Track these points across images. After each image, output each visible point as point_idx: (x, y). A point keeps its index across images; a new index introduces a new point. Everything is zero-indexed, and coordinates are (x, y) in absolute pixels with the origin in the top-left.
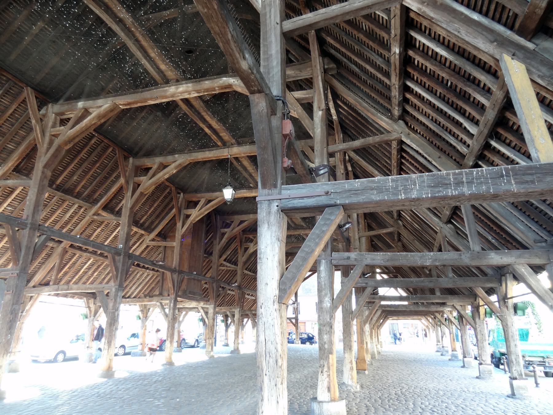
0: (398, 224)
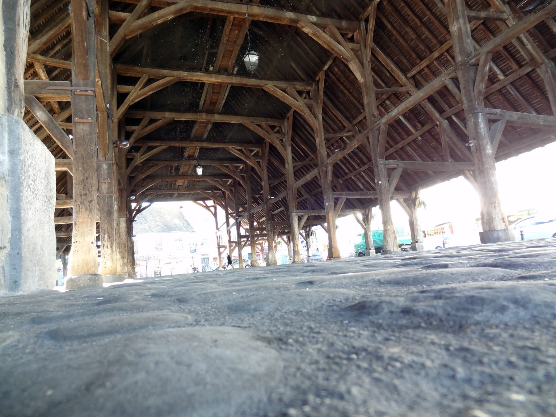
0: (355, 129)
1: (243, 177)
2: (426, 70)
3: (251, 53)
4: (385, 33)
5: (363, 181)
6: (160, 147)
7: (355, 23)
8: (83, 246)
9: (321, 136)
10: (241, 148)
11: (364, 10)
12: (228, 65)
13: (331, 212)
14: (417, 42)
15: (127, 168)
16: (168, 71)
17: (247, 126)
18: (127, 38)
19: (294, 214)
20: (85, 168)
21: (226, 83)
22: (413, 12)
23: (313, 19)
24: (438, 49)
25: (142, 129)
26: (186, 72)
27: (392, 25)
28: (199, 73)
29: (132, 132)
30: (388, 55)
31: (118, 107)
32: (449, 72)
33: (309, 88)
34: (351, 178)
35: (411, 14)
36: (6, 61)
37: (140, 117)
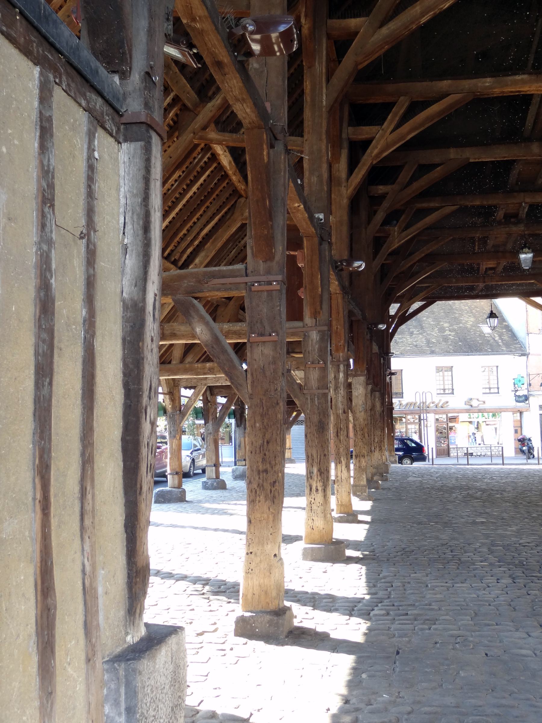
8: (261, 562)
15: (374, 260)
16: (449, 81)
18: (360, 67)
20: (265, 424)
25: (402, 190)
26: (489, 80)
28: (518, 77)
36: (127, 546)
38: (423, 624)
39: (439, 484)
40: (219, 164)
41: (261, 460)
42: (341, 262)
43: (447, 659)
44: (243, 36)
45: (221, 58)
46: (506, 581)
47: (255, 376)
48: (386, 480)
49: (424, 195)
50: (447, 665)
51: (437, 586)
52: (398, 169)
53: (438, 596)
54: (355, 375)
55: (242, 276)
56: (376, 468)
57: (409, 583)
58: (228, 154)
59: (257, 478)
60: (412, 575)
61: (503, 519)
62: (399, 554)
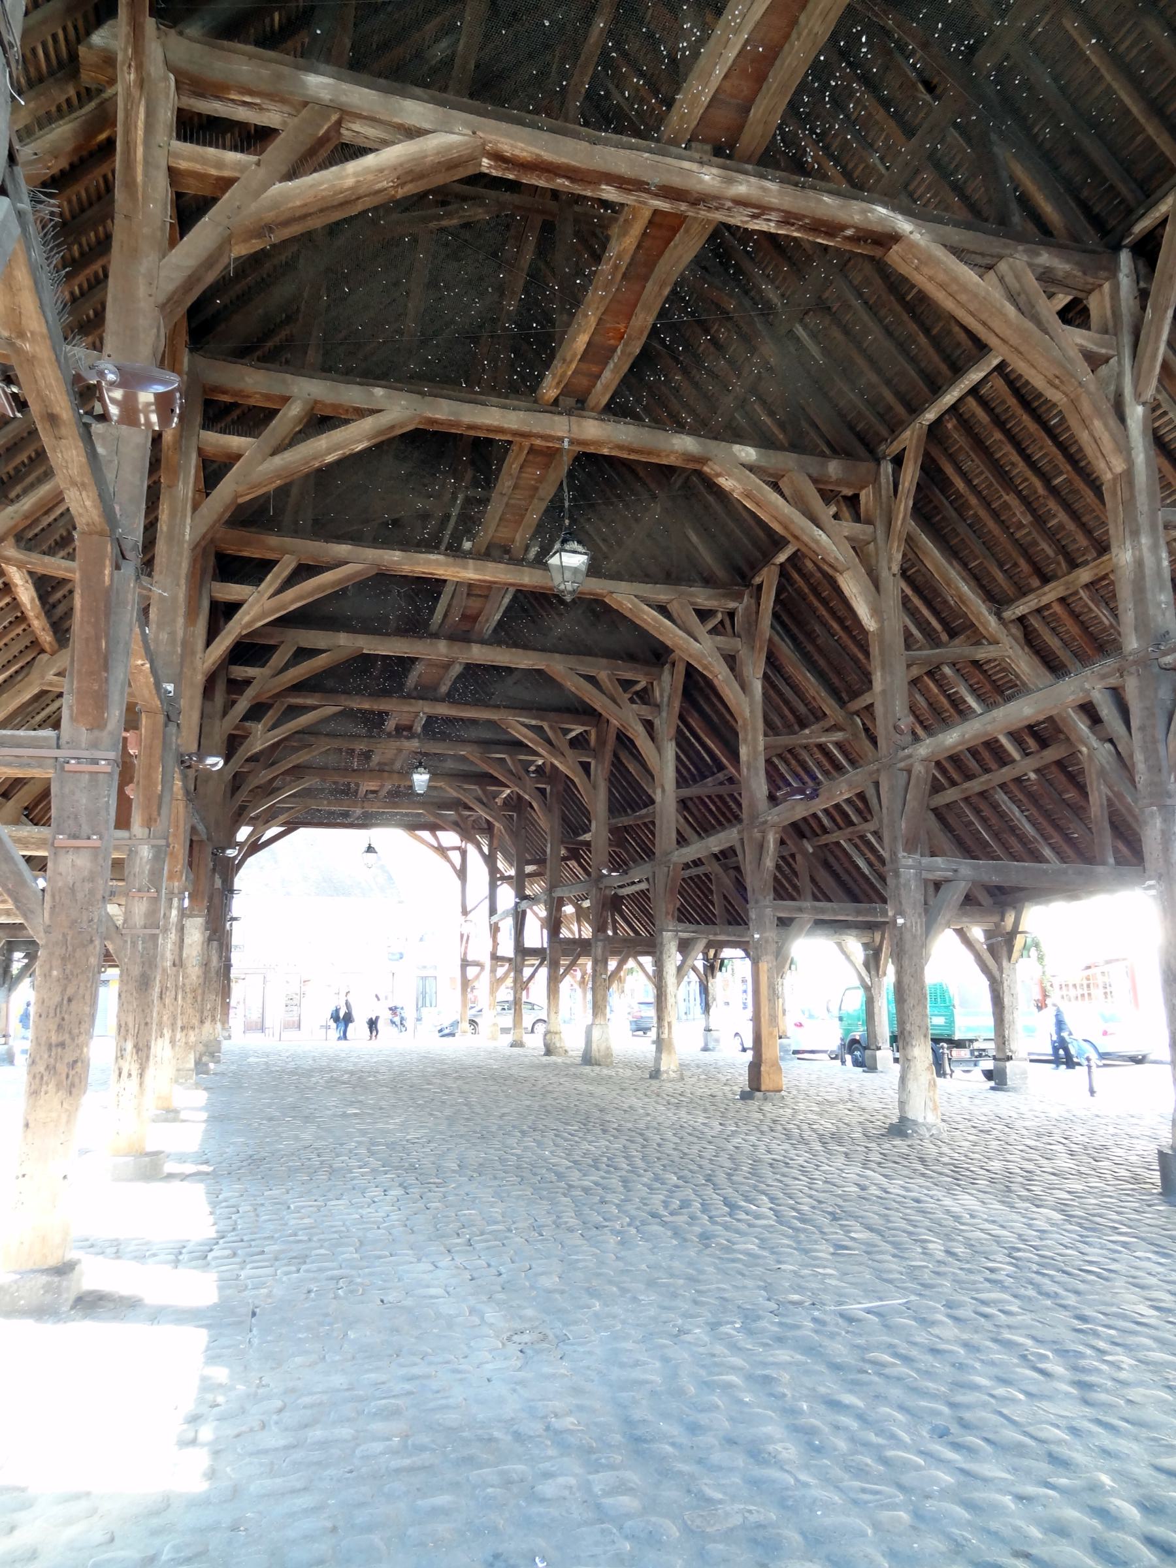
0: (854, 723)
1: (542, 791)
2: (1057, 608)
3: (567, 547)
4: (947, 498)
5: (869, 855)
6: (323, 709)
7: (865, 467)
9: (755, 739)
10: (539, 723)
11: (893, 431)
12: (513, 541)
13: (764, 958)
14: (1035, 534)
17: (559, 680)
18: (240, 501)
19: (667, 935)
20: (68, 971)
21: (505, 584)
22: (1027, 458)
23: (747, 454)
24: (1092, 565)
26: (398, 553)
27: (968, 482)
28: (432, 557)
29: (248, 682)
30: (953, 552)
31: (208, 643)
32: (1102, 672)
33: (732, 605)
34: (838, 844)
35: (1021, 464)
37: (272, 642)
38: (289, 1265)
39: (291, 1065)
40: (15, 599)
41: (55, 1027)
42: (190, 755)
43: (327, 1315)
44: (98, 386)
45: (57, 410)
46: (397, 1192)
47: (57, 898)
48: (218, 1062)
49: (299, 687)
50: (329, 1324)
51: (303, 1207)
52: (272, 649)
53: (306, 1221)
54: (191, 916)
55: (49, 748)
56: (206, 1045)
57: (262, 1205)
58: (31, 587)
59: (46, 1056)
60: (266, 1193)
61: (381, 1109)
62: (245, 1163)
